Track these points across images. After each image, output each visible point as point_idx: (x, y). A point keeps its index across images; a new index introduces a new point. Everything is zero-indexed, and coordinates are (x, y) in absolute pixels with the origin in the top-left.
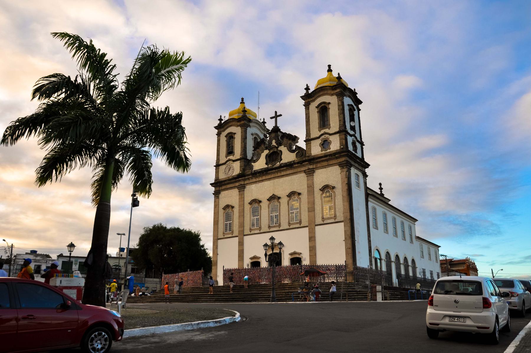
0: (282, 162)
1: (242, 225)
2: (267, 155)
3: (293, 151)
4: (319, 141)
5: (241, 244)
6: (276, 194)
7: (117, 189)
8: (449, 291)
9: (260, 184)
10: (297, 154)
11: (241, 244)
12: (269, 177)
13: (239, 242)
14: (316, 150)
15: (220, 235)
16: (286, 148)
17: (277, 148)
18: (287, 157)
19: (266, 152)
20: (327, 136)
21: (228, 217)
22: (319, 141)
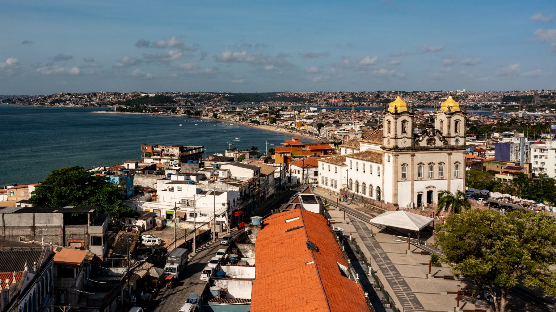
0: (435, 145)
1: (413, 176)
2: (427, 139)
3: (441, 141)
4: (454, 139)
5: (412, 185)
6: (337, 182)
7: (248, 258)
8: (402, 211)
9: (422, 155)
10: (444, 142)
11: (412, 185)
12: (429, 152)
13: (411, 184)
14: (452, 142)
15: (400, 179)
16: (438, 138)
17: (433, 137)
18: (439, 143)
19: (427, 137)
20: (458, 137)
21: (404, 170)
22: (454, 139)
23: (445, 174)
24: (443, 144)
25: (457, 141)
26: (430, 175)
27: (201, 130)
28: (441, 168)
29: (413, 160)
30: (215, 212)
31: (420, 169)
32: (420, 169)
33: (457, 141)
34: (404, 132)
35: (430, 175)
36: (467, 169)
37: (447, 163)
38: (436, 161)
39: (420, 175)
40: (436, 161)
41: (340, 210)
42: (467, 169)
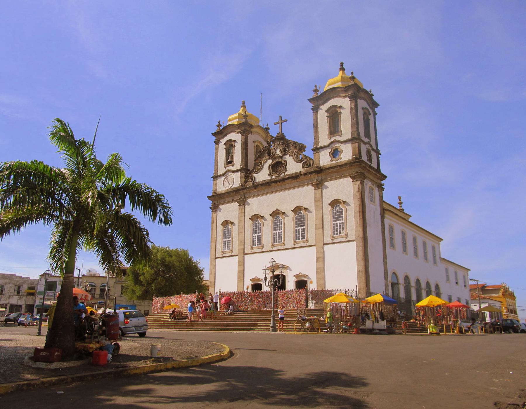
4: (328, 150)
5: (241, 263)
11: (241, 263)
19: (270, 162)
22: (328, 150)
23: (312, 234)
24: (303, 167)
25: (335, 153)
26: (278, 238)
27: (393, 211)
28: (300, 222)
29: (243, 214)
30: (217, 215)
31: (257, 229)
32: (257, 229)
33: (335, 153)
34: (229, 162)
35: (278, 238)
36: (155, 194)
37: (312, 208)
38: (287, 207)
39: (257, 241)
40: (287, 207)
41: (290, 156)
42: (155, 194)
